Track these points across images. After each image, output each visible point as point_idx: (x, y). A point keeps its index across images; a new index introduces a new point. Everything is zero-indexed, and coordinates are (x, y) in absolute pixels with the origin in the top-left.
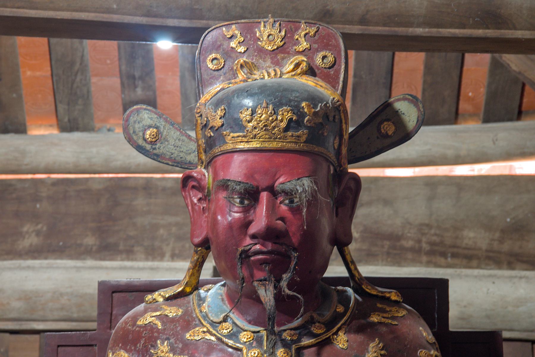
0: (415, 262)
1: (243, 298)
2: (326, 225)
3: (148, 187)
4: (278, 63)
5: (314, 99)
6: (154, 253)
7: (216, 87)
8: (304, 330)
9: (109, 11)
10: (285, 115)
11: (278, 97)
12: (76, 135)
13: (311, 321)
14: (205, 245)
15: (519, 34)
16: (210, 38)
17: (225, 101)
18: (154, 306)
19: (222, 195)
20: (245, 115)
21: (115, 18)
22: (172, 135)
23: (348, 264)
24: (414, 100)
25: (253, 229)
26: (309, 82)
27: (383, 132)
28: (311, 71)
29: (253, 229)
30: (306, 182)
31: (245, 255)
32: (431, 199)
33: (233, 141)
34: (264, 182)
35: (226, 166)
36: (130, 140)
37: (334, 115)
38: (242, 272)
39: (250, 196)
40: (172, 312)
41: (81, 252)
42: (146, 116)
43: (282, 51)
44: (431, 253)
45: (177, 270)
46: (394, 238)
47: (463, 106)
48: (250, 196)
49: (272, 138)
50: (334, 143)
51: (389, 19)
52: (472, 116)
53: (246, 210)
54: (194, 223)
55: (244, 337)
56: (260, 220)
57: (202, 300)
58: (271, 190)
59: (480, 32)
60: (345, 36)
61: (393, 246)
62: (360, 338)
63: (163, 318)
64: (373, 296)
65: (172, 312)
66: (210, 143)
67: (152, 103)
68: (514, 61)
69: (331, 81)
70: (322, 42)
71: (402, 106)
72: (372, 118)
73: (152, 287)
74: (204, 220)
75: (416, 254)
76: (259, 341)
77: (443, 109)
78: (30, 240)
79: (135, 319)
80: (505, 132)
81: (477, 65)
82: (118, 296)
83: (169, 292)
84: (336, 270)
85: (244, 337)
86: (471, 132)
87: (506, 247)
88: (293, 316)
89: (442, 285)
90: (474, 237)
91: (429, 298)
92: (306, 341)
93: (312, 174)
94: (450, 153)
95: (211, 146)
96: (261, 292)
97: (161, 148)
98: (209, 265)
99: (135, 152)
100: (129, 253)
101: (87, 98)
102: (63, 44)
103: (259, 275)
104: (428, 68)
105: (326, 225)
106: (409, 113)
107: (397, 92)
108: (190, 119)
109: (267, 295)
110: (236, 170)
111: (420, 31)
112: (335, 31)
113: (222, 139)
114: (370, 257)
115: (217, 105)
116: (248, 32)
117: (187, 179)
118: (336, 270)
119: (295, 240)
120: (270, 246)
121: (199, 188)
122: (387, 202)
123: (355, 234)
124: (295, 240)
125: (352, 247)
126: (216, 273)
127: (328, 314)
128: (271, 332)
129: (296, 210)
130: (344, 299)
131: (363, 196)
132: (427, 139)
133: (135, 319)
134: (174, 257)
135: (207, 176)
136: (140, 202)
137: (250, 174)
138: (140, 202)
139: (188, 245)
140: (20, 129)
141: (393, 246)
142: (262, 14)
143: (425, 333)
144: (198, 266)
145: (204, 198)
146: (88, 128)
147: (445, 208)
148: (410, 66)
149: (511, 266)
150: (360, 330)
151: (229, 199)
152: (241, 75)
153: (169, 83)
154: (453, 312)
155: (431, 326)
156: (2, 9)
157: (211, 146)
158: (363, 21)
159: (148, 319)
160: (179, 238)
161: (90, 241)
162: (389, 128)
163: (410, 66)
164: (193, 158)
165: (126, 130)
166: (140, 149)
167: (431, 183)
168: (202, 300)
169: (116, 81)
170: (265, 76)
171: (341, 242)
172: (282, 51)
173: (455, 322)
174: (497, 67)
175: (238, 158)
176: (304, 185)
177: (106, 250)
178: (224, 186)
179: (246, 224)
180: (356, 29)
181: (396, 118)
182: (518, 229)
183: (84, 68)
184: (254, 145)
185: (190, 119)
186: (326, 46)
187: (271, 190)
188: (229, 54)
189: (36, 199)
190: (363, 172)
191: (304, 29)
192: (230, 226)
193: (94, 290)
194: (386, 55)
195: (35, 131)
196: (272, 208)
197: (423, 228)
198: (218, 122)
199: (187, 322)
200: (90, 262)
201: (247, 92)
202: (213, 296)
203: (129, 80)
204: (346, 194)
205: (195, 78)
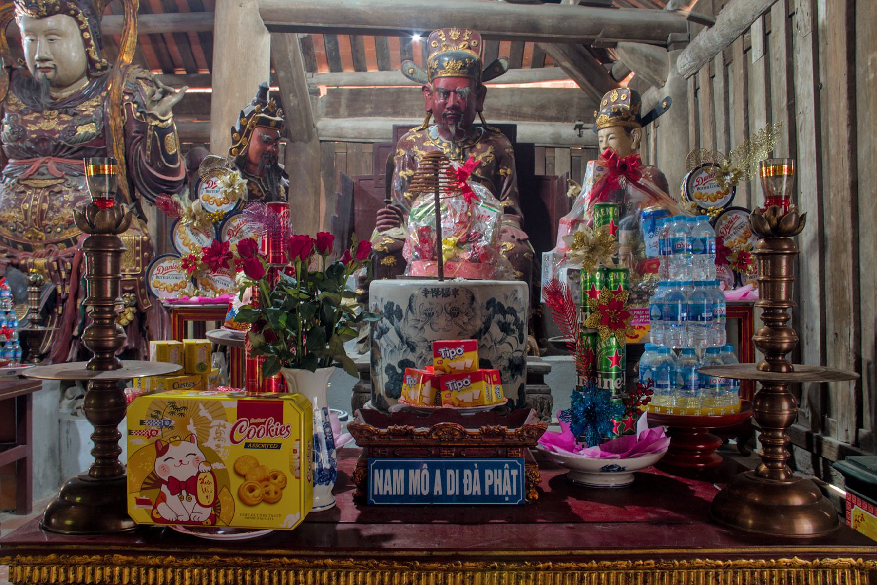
0: (506, 119)
1: (444, 131)
2: (474, 105)
3: (410, 91)
4: (457, 45)
5: (470, 58)
6: (412, 115)
7: (435, 53)
8: (465, 142)
9: (397, 25)
10: (460, 64)
11: (457, 57)
12: (384, 72)
13: (468, 139)
14: (431, 111)
15: (545, 35)
16: (432, 35)
17: (438, 59)
18: (412, 133)
19: (437, 93)
20: (445, 64)
21: (399, 28)
22: (419, 71)
23: (482, 119)
24: (506, 59)
25: (448, 106)
26: (469, 52)
27: (495, 70)
28: (469, 48)
29: (448, 106)
30: (467, 89)
31: (445, 115)
32: (512, 96)
33: (442, 73)
34: (452, 89)
35: (439, 82)
36: (404, 73)
37: (476, 64)
38: (444, 121)
39: (447, 94)
40: (419, 136)
41: (386, 115)
42: (410, 64)
43: (459, 40)
44: (511, 115)
45: (420, 121)
46: (498, 110)
47: (524, 62)
48: (447, 94)
49: (455, 72)
50: (477, 74)
51: (498, 29)
52: (527, 65)
53: (445, 99)
54: (426, 104)
55: (445, 145)
56: (451, 102)
57: (429, 131)
58: (454, 91)
59: (530, 34)
60: (482, 35)
61: (498, 112)
62: (485, 145)
63: (415, 138)
64: (491, 130)
65: (419, 136)
66: (433, 74)
67: (412, 59)
68: (542, 45)
69: (477, 51)
70: (473, 37)
71: (502, 61)
72: (491, 65)
73: (412, 127)
74: (430, 102)
75: (506, 116)
76: (449, 146)
77: (517, 62)
78: (369, 110)
79: (406, 138)
80: (539, 72)
81: (529, 47)
82: (400, 130)
83: (417, 128)
84: (477, 121)
85: (445, 145)
86: (527, 71)
87: (538, 113)
88: (462, 137)
89: (514, 127)
90: (526, 110)
91: (510, 131)
92: (466, 146)
93: (469, 86)
94: (519, 79)
95: (433, 74)
96: (451, 129)
97: (415, 76)
98: (432, 120)
99: (406, 78)
100: (403, 115)
101: (388, 58)
102: (381, 38)
103: (450, 122)
104: (512, 48)
105: (474, 105)
106: (505, 64)
107: (500, 56)
108: (426, 66)
109: (452, 130)
110: (442, 84)
111: (509, 33)
112: (479, 33)
113: (437, 73)
114: (490, 117)
115: (435, 60)
116: (447, 33)
117: (424, 87)
118: (477, 121)
119: (463, 110)
120: (454, 112)
121: (428, 90)
122: (496, 97)
123: (485, 108)
124: (463, 110)
125: (483, 113)
126: (434, 122)
127: (474, 137)
128: (454, 143)
129: (463, 99)
130: (480, 131)
131: (488, 94)
132: (511, 74)
133: (406, 138)
134: (419, 116)
135: (431, 86)
136: (407, 96)
137: (447, 86)
138: (407, 96)
139: (425, 112)
140: (365, 70)
141: (498, 112)
142: (452, 26)
143: (508, 144)
144: (428, 119)
145: (431, 94)
146: (389, 69)
147: (517, 99)
148: (505, 47)
149: (539, 120)
150: (485, 142)
151: (439, 95)
152: (444, 49)
153: (418, 53)
154: (518, 137)
155: (510, 140)
156: (875, 550)
157: (433, 74)
158: (488, 29)
159: (410, 138)
160: (421, 110)
161: (390, 110)
162: (497, 69)
163: (505, 47)
164: (426, 80)
165: (402, 69)
166: (407, 76)
167: (512, 90)
168: (429, 131)
169: (399, 52)
170: (453, 49)
171: (479, 111)
172: (459, 40)
173: (519, 139)
174: (536, 47)
175: (442, 80)
176: (466, 90)
177: (395, 114)
178: (438, 90)
179: (445, 104)
180: (486, 32)
181: (500, 65)
182: (542, 107)
183: (387, 48)
184: (449, 75)
185: (426, 66)
186: (475, 39)
187: (454, 91)
188: (440, 41)
189: (371, 95)
190: (487, 86)
191: (467, 32)
192: (440, 105)
193: (391, 128)
194: (497, 42)
195: (370, 71)
196: (455, 98)
197: (509, 106)
198: (435, 66)
199: (424, 139)
200: (390, 118)
201: (446, 55)
202: (433, 130)
203: (403, 52)
204: (481, 93)
205: (427, 49)
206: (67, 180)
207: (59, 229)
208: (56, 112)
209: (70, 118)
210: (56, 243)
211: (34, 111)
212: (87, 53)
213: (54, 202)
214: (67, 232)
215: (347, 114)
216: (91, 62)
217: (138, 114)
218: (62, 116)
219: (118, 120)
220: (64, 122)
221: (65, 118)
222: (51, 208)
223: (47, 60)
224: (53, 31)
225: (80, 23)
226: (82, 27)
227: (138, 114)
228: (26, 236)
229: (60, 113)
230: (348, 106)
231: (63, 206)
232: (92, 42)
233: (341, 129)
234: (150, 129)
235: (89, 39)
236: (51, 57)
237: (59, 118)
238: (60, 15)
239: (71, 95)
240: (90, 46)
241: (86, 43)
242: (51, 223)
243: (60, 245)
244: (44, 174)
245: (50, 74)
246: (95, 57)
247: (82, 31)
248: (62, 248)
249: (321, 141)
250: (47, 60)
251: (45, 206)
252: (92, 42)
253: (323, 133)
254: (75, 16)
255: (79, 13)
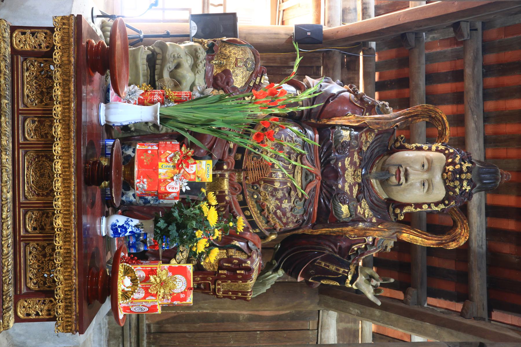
206: (301, 199)
207: (256, 197)
208: (360, 181)
209: (355, 195)
210: (242, 193)
211: (361, 160)
212: (410, 205)
213: (281, 192)
214: (253, 203)
215: (340, 328)
216: (402, 206)
217: (356, 249)
218: (357, 187)
219: (352, 233)
220: (351, 190)
221: (355, 190)
222: (276, 189)
223: (406, 180)
224: (431, 187)
225: (437, 204)
226: (432, 205)
227: (356, 249)
228: (248, 163)
229: (359, 184)
230: (346, 329)
231: (277, 199)
232: (419, 210)
233: (328, 329)
234: (344, 272)
235: (421, 208)
236: (409, 183)
237: (354, 185)
238: (445, 193)
239: (372, 187)
240: (415, 208)
241: (418, 205)
242: (261, 189)
243: (241, 196)
244: (306, 180)
245: (394, 179)
246: (406, 210)
247: (429, 205)
248: (238, 197)
249: (319, 311)
250: (406, 180)
251: (277, 185)
252: (419, 210)
253: (325, 314)
254: (442, 202)
255: (445, 206)
